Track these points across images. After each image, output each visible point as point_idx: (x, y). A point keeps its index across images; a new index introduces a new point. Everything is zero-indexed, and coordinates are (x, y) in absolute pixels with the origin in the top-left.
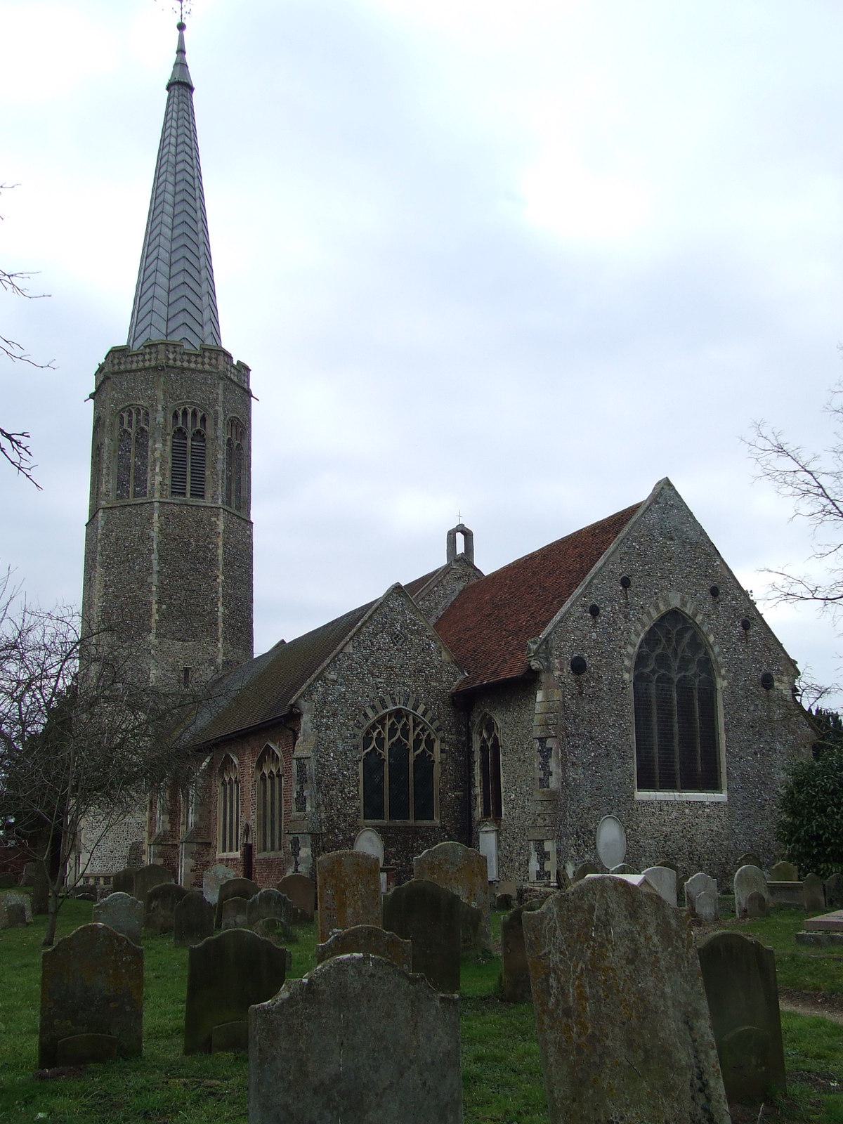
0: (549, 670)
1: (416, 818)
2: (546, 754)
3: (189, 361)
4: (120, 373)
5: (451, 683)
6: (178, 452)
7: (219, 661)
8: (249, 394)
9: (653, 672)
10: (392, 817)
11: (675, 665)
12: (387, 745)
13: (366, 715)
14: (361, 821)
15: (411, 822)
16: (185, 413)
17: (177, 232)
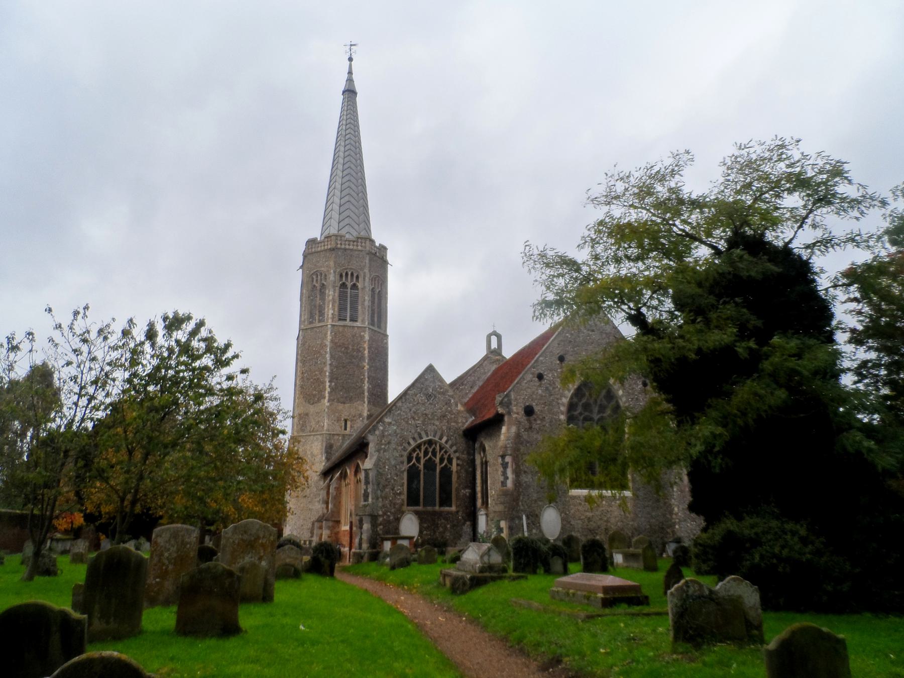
0: (509, 413)
1: (441, 505)
2: (505, 466)
4: (312, 253)
5: (464, 423)
6: (342, 297)
9: (581, 414)
10: (424, 505)
11: (596, 409)
13: (409, 443)
14: (405, 508)
15: (437, 508)
16: (347, 274)
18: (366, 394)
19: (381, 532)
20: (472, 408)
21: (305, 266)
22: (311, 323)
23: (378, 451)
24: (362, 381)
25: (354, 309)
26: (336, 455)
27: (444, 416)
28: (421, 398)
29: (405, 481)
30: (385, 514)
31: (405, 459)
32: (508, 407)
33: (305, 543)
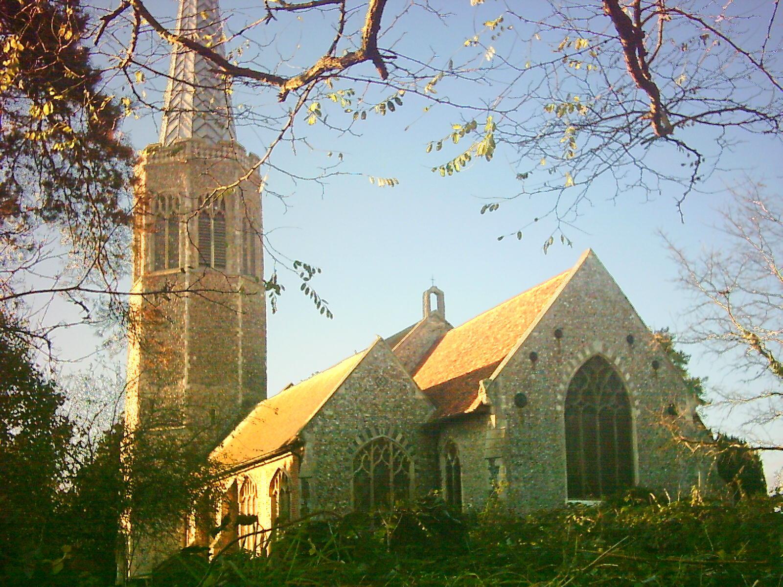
6: (204, 231)
9: (581, 404)
11: (598, 398)
12: (372, 466)
13: (355, 443)
18: (240, 372)
22: (157, 268)
25: (221, 247)
31: (350, 464)
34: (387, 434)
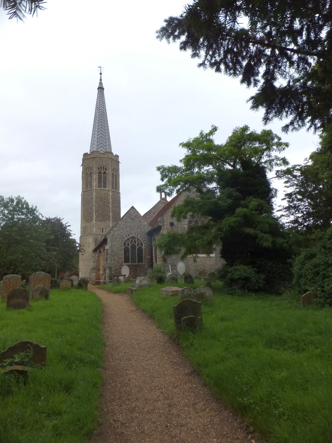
0: (163, 225)
3: (102, 155)
4: (86, 159)
7: (111, 226)
8: (119, 162)
12: (130, 245)
13: (124, 238)
14: (123, 264)
16: (101, 168)
17: (99, 124)
18: (111, 218)
19: (113, 274)
20: (150, 224)
21: (83, 165)
22: (87, 189)
23: (111, 242)
24: (109, 212)
26: (98, 244)
27: (139, 227)
28: (129, 220)
29: (123, 253)
30: (115, 266)
32: (163, 223)
33: (88, 279)
34: (135, 235)
